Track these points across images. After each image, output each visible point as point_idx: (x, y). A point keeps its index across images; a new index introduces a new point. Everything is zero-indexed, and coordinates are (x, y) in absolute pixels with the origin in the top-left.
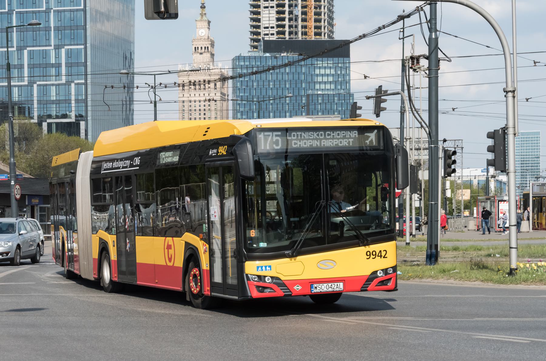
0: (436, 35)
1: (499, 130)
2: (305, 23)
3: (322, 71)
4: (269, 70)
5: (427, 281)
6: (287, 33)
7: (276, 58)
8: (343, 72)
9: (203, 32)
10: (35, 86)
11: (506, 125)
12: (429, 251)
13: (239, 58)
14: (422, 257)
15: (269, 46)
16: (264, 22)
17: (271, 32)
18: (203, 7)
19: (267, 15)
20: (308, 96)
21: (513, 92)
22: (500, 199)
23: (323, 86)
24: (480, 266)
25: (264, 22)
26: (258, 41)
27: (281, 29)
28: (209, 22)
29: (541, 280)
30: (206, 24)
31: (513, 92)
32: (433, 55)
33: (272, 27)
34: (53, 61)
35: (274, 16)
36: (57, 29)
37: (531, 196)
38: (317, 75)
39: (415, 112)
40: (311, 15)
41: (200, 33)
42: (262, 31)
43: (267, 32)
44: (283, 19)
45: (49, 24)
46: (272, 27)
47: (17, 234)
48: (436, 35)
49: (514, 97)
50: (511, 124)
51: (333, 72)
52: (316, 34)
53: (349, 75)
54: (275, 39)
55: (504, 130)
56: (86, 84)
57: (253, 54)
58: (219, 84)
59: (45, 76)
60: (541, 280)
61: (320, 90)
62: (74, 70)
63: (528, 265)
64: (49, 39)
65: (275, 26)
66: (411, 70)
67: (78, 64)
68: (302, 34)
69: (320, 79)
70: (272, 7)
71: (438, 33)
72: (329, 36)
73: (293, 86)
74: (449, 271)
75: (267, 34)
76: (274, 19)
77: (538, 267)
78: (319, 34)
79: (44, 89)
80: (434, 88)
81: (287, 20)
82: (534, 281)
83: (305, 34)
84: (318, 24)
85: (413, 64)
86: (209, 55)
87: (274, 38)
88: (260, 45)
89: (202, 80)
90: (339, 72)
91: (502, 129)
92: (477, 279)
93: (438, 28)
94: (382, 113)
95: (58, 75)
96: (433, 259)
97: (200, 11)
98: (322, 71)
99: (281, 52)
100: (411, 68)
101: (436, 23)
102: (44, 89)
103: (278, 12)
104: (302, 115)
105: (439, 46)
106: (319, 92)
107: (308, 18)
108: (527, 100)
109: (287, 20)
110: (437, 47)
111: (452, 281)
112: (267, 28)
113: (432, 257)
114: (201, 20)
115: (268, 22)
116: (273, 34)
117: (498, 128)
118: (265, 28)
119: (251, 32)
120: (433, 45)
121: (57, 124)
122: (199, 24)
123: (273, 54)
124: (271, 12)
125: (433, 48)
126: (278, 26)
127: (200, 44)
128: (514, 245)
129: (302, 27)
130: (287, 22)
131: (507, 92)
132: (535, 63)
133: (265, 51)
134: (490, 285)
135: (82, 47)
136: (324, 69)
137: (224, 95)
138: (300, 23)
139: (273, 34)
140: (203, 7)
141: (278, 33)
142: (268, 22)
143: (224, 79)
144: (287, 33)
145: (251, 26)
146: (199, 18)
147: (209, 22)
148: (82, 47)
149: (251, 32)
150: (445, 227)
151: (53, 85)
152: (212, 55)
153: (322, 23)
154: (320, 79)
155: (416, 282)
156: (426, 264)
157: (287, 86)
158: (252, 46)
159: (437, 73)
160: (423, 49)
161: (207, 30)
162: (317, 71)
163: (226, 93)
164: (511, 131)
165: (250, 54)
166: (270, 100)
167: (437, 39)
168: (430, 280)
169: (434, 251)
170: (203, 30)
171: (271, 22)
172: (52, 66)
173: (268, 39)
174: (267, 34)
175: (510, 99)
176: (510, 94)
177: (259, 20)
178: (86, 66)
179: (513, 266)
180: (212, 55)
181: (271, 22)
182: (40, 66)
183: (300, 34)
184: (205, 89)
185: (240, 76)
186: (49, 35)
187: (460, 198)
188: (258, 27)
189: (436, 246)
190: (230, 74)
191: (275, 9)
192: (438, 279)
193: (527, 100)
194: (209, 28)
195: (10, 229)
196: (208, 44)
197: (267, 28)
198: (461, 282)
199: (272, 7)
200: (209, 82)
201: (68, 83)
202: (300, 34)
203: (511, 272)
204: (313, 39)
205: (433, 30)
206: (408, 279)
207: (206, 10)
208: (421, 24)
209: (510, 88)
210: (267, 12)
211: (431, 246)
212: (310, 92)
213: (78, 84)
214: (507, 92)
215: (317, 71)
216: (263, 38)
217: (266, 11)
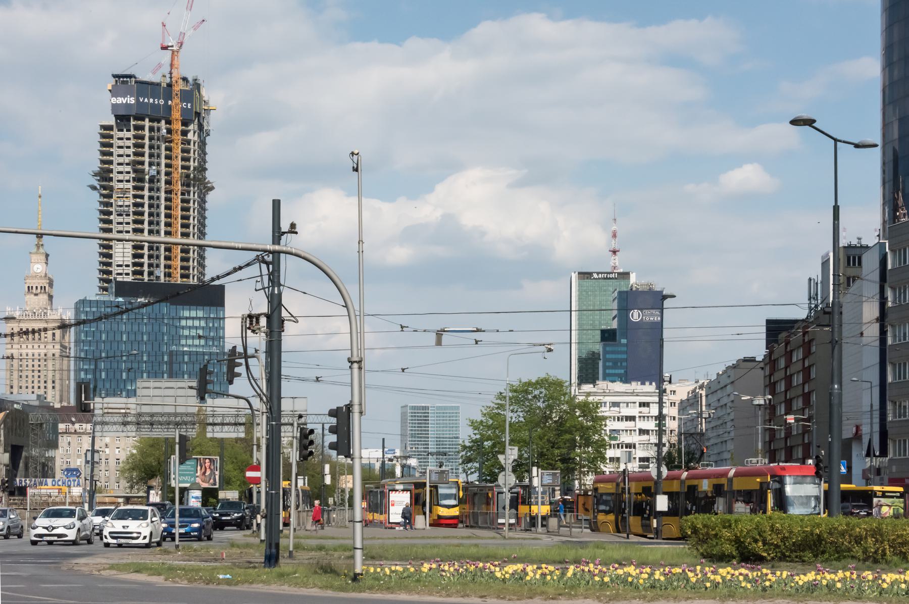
0: (279, 290)
1: (342, 408)
2: (169, 262)
4: (100, 319)
5: (259, 588)
6: (146, 274)
8: (216, 325)
9: (38, 268)
11: (351, 401)
12: (268, 550)
13: (83, 302)
14: (259, 556)
15: (122, 289)
16: (117, 259)
17: (126, 271)
19: (121, 250)
20: (171, 354)
21: (359, 362)
22: (391, 488)
23: (190, 342)
24: (328, 570)
25: (117, 258)
26: (108, 281)
27: (139, 268)
28: (47, 256)
29: (388, 588)
30: (43, 257)
31: (359, 362)
32: (276, 314)
33: (127, 266)
37: (428, 485)
38: (183, 328)
39: (252, 381)
41: (35, 269)
42: (114, 269)
43: (121, 271)
44: (142, 256)
46: (127, 266)
47: (149, 520)
48: (279, 290)
49: (360, 368)
50: (356, 401)
51: (203, 323)
52: (182, 276)
53: (223, 328)
54: (129, 280)
55: (349, 407)
57: (102, 298)
58: (58, 333)
60: (388, 588)
61: (186, 345)
63: (379, 570)
65: (130, 263)
66: (249, 332)
68: (165, 276)
69: (186, 332)
71: (281, 288)
72: (199, 279)
74: (288, 575)
75: (121, 274)
76: (130, 255)
77: (392, 572)
78: (187, 276)
80: (275, 354)
81: (146, 257)
82: (380, 589)
83: (168, 275)
84: (185, 264)
85: (251, 324)
86: (46, 297)
87: (129, 279)
88: (112, 287)
89: (30, 329)
90: (211, 325)
91: (346, 406)
92: (315, 586)
93: (282, 282)
94: (236, 380)
96: (273, 561)
99: (138, 297)
100: (249, 328)
101: (279, 276)
104: (142, 377)
105: (283, 303)
106: (185, 349)
107: (173, 256)
108: (403, 370)
109: (146, 257)
110: (280, 304)
111: (286, 587)
112: (121, 266)
113: (272, 559)
114: (36, 253)
115: (121, 259)
116: (127, 274)
117: (341, 404)
118: (118, 266)
119: (100, 271)
120: (275, 302)
122: (34, 258)
124: (126, 246)
125: (275, 306)
126: (135, 264)
127: (35, 283)
128: (358, 544)
129: (165, 267)
130: (145, 260)
131: (352, 363)
132: (402, 327)
133: (117, 295)
134: (329, 593)
136: (192, 319)
137: (65, 348)
138: (163, 262)
139: (127, 274)
141: (135, 273)
142: (121, 259)
143: (64, 326)
144: (146, 274)
145: (100, 263)
147: (47, 256)
149: (100, 271)
150: (319, 521)
152: (51, 297)
153: (191, 263)
154: (186, 332)
155: (244, 588)
156: (265, 567)
157: (124, 339)
158: (100, 288)
159: (280, 336)
160: (262, 307)
161: (45, 265)
163: (67, 345)
164: (356, 409)
165: (97, 298)
166: (122, 356)
167: (280, 294)
168: (260, 585)
169: (274, 550)
170: (39, 266)
171: (125, 259)
173: (121, 280)
174: (121, 274)
175: (356, 371)
176: (356, 366)
177: (110, 256)
179: (358, 571)
180: (51, 297)
181: (125, 259)
184: (40, 339)
185: (84, 322)
187: (344, 486)
188: (110, 264)
189: (277, 545)
190: (73, 322)
192: (269, 585)
193: (403, 370)
194: (47, 263)
195: (4, 514)
196: (44, 282)
197: (121, 266)
198: (296, 589)
200: (45, 330)
203: (355, 578)
204: (179, 282)
205: (276, 284)
206: (236, 584)
208: (261, 276)
209: (355, 359)
210: (121, 246)
211: (270, 545)
212: (174, 348)
214: (352, 363)
216: (115, 279)
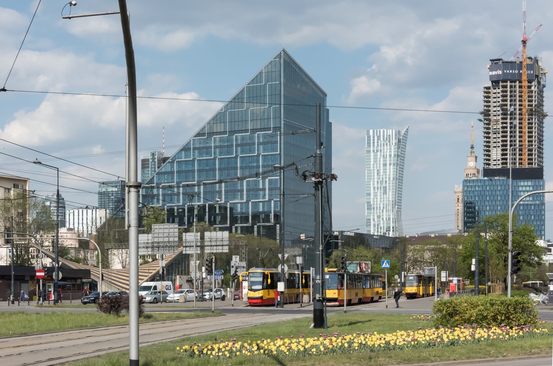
3: (524, 189)
7: (491, 180)
10: (272, 201)
18: (472, 147)
28: (476, 157)
30: (474, 158)
33: (499, 160)
34: (261, 187)
35: (500, 152)
36: (199, 171)
38: (520, 191)
40: (526, 151)
44: (506, 155)
45: (194, 168)
46: (499, 160)
52: (529, 164)
56: (280, 201)
59: (257, 197)
62: (274, 192)
64: (194, 178)
67: (275, 189)
70: (499, 147)
73: (503, 198)
78: (532, 164)
79: (255, 204)
83: (521, 164)
84: (530, 157)
87: (500, 167)
95: (264, 196)
97: (470, 150)
98: (524, 189)
102: (255, 204)
103: (503, 150)
107: (523, 153)
116: (499, 165)
118: (494, 160)
121: (241, 227)
122: (469, 159)
123: (490, 178)
135: (278, 177)
139: (499, 165)
140: (472, 147)
141: (503, 164)
145: (485, 159)
146: (470, 155)
147: (476, 157)
148: (278, 177)
151: (261, 202)
153: (534, 156)
162: (520, 189)
172: (261, 190)
177: (489, 156)
178: (280, 190)
182: (253, 190)
183: (518, 164)
186: (174, 176)
188: (489, 160)
191: (501, 148)
194: (476, 161)
199: (499, 147)
201: (270, 201)
202: (518, 164)
207: (474, 150)
213: (276, 201)
215: (520, 189)
217: (495, 149)
